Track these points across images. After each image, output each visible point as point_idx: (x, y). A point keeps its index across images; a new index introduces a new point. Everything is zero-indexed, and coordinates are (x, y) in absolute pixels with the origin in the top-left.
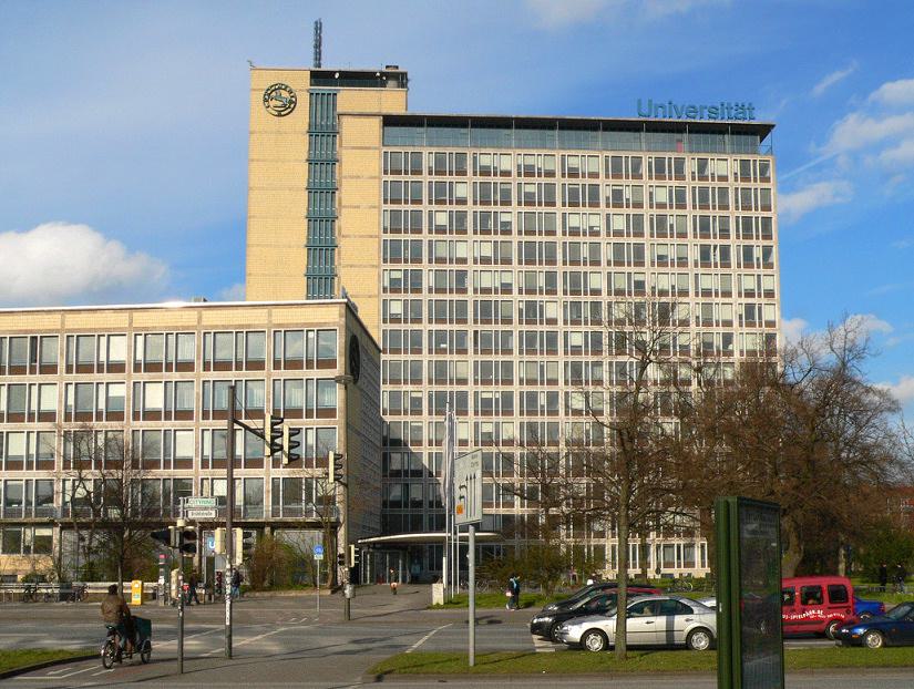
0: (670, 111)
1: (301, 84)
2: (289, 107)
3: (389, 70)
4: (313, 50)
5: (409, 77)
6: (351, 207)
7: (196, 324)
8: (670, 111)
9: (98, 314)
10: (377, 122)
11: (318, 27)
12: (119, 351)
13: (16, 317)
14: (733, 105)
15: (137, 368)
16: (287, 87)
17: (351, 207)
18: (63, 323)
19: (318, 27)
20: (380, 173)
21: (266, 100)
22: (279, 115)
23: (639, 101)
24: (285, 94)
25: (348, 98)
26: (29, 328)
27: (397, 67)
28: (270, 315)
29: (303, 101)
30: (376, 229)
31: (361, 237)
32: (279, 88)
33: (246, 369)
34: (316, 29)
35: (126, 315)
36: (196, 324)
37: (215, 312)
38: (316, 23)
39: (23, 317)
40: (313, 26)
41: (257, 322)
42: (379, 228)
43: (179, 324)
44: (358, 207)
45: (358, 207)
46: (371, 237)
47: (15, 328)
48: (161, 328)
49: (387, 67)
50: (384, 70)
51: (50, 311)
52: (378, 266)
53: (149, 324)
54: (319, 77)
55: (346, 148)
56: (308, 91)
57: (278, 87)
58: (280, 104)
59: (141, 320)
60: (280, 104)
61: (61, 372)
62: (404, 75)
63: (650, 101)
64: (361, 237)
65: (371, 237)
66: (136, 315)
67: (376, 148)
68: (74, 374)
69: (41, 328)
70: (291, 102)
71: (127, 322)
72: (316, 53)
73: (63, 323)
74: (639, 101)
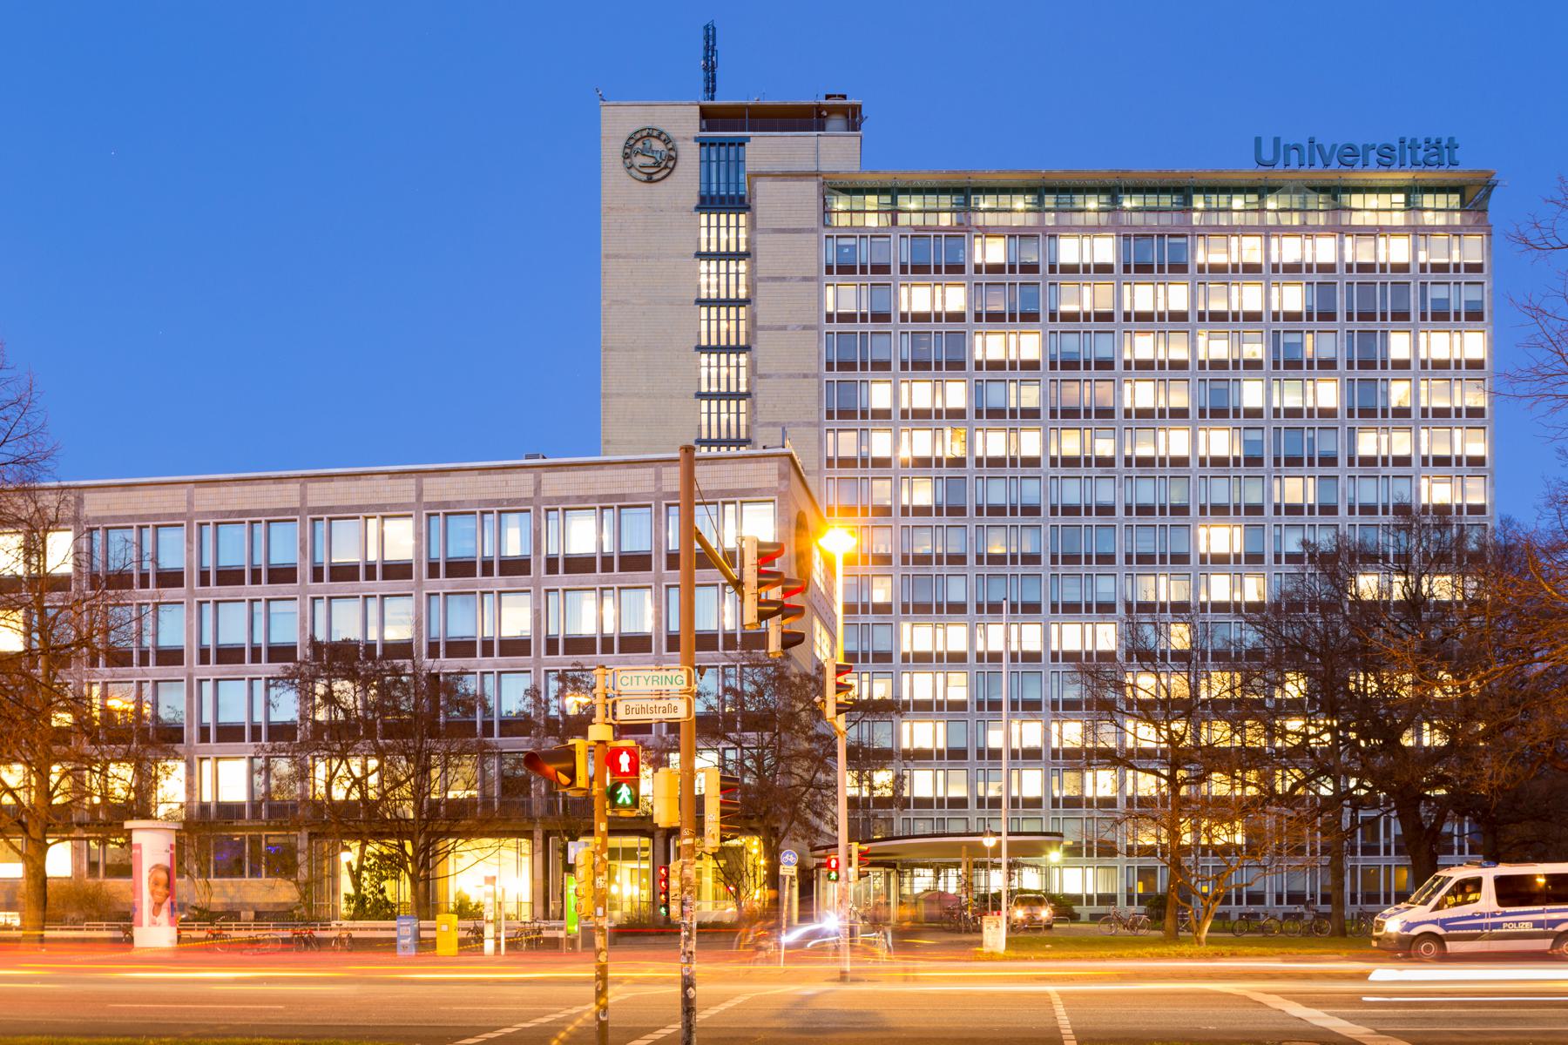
0: (1312, 156)
1: (682, 122)
2: (666, 165)
3: (830, 102)
4: (701, 75)
5: (864, 113)
6: (770, 328)
7: (532, 495)
8: (1312, 156)
9: (362, 483)
10: (811, 188)
11: (710, 35)
12: (174, 552)
13: (223, 489)
14: (1421, 141)
15: (433, 571)
16: (662, 133)
17: (770, 328)
18: (303, 497)
19: (710, 35)
20: (819, 270)
21: (626, 156)
22: (650, 180)
23: (1258, 141)
24: (658, 145)
25: (763, 149)
26: (246, 507)
27: (844, 97)
28: (658, 478)
29: (690, 155)
30: (816, 365)
31: (790, 376)
32: (649, 135)
33: (621, 570)
34: (707, 38)
35: (410, 484)
36: (532, 495)
37: (563, 474)
38: (707, 28)
39: (235, 489)
40: (701, 34)
41: (635, 491)
42: (819, 364)
43: (505, 496)
44: (784, 328)
45: (784, 328)
46: (805, 376)
47: (223, 508)
48: (471, 503)
49: (828, 97)
50: (824, 102)
51: (280, 478)
52: (818, 425)
53: (451, 497)
54: (710, 117)
55: (764, 231)
56: (696, 139)
57: (651, 134)
58: (650, 161)
59: (437, 489)
60: (650, 161)
61: (304, 580)
62: (856, 109)
63: (1277, 141)
64: (790, 376)
65: (805, 376)
66: (428, 482)
67: (812, 231)
68: (264, 585)
69: (266, 506)
70: (670, 158)
71: (414, 494)
72: (707, 80)
73: (303, 497)
74: (1258, 141)
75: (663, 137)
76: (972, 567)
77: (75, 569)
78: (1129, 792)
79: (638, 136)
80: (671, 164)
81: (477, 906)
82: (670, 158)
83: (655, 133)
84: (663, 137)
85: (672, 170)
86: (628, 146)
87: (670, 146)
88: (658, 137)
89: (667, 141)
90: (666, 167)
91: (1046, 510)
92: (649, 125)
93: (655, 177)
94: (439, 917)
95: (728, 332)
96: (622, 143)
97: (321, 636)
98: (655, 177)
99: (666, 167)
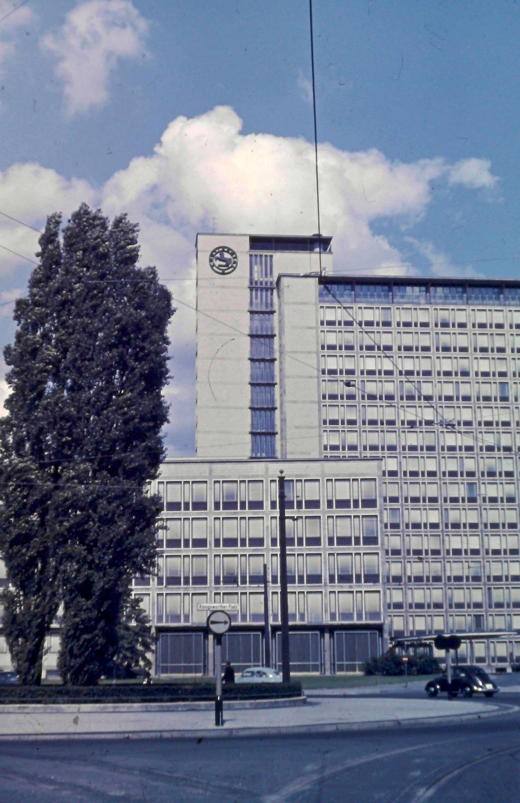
21: (211, 261)
22: (223, 273)
24: (227, 256)
29: (243, 260)
73: (488, 648)
75: (230, 252)
76: (358, 377)
77: (137, 622)
78: (411, 628)
79: (217, 251)
80: (234, 265)
81: (118, 222)
82: (235, 263)
83: (226, 250)
84: (230, 252)
85: (235, 268)
86: (212, 255)
87: (234, 256)
88: (228, 252)
89: (233, 253)
90: (232, 267)
91: (395, 348)
92: (222, 245)
93: (226, 272)
94: (104, 214)
95: (256, 298)
96: (209, 253)
97: (165, 531)
98: (226, 272)
99: (232, 267)
